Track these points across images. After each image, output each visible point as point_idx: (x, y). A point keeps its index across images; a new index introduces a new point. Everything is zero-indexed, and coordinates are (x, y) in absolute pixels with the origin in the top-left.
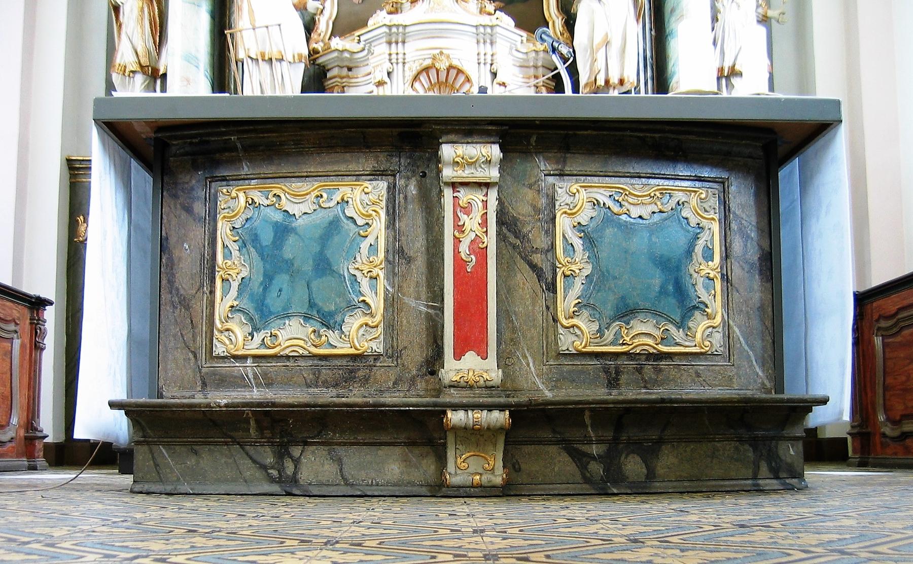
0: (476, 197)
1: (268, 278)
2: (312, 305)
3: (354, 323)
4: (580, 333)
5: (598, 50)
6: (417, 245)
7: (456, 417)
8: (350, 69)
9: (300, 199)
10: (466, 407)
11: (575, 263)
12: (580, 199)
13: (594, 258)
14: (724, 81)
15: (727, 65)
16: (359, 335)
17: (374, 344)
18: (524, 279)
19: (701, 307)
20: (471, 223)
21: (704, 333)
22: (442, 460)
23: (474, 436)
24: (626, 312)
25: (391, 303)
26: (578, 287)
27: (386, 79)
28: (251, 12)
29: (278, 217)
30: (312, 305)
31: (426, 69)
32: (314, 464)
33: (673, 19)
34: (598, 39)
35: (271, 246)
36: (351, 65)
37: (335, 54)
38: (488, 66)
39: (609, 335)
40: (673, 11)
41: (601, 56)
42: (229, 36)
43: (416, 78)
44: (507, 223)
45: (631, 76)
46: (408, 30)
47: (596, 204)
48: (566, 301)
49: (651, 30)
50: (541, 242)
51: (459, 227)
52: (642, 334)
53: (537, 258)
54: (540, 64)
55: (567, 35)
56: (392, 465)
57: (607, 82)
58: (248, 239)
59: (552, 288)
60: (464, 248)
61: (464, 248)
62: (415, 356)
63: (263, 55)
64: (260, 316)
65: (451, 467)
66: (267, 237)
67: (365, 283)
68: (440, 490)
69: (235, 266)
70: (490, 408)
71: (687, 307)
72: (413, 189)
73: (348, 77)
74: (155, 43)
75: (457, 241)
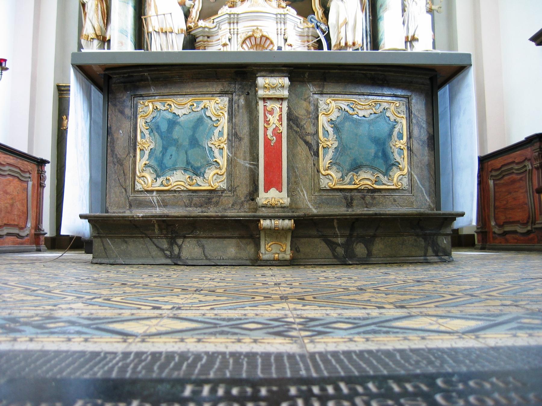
0: (276, 106)
1: (165, 149)
2: (188, 163)
3: (210, 173)
4: (331, 178)
5: (341, 27)
6: (244, 131)
7: (265, 223)
8: (208, 37)
9: (182, 107)
10: (271, 218)
11: (329, 141)
12: (331, 106)
13: (339, 138)
14: (408, 44)
15: (410, 35)
16: (213, 179)
17: (221, 184)
18: (302, 150)
19: (396, 164)
20: (273, 119)
21: (398, 178)
22: (258, 246)
23: (275, 234)
24: (356, 167)
25: (230, 162)
26: (330, 154)
27: (228, 42)
28: (156, 6)
29: (170, 116)
30: (188, 163)
31: (249, 37)
32: (189, 248)
33: (381, 11)
34: (341, 21)
35: (165, 132)
36: (209, 35)
37: (201, 29)
38: (283, 35)
39: (347, 179)
40: (381, 6)
41: (343, 30)
42: (144, 19)
43: (244, 42)
44: (292, 119)
45: (359, 40)
46: (239, 16)
47: (340, 109)
48: (324, 161)
49: (370, 16)
50: (310, 129)
51: (267, 122)
52: (365, 179)
53: (309, 138)
54: (310, 34)
55: (324, 19)
56: (231, 249)
57: (346, 44)
58: (154, 128)
59: (317, 154)
60: (270, 133)
61: (270, 133)
62: (243, 191)
63: (162, 30)
64: (160, 169)
65: (262, 250)
66: (164, 127)
67: (216, 152)
68: (257, 262)
69: (147, 142)
70: (284, 218)
71: (388, 164)
72: (242, 102)
73: (207, 41)
74: (104, 23)
75: (266, 129)
